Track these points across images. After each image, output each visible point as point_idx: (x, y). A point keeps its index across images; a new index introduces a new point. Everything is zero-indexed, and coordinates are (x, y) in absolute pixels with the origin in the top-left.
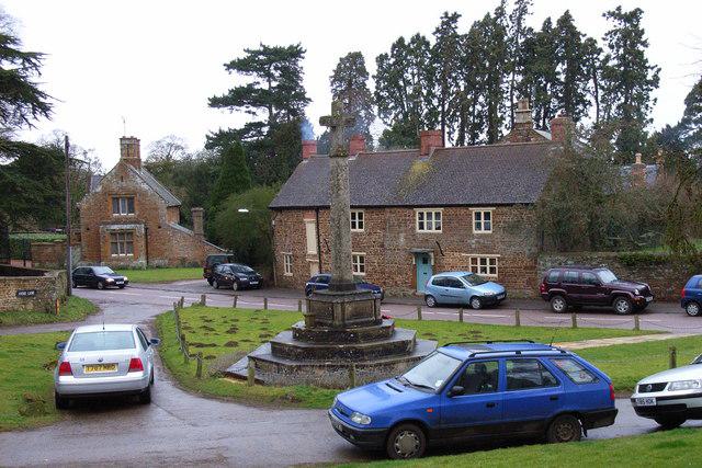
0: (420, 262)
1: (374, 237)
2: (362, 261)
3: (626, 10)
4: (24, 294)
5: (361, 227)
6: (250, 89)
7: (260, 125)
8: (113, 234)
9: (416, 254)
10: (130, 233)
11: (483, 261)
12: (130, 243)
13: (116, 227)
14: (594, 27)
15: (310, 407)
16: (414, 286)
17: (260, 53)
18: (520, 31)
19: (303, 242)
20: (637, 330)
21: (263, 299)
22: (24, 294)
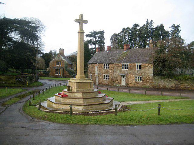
0: (122, 77)
1: (111, 71)
2: (108, 77)
3: (176, 25)
4: (18, 79)
5: (108, 68)
6: (91, 41)
7: (93, 48)
8: (56, 70)
9: (121, 75)
10: (59, 70)
11: (139, 78)
12: (59, 72)
13: (56, 68)
14: (168, 28)
15: (47, 120)
16: (121, 84)
17: (93, 33)
18: (152, 29)
19: (94, 72)
20: (71, 105)
21: (118, 89)
22: (18, 79)
